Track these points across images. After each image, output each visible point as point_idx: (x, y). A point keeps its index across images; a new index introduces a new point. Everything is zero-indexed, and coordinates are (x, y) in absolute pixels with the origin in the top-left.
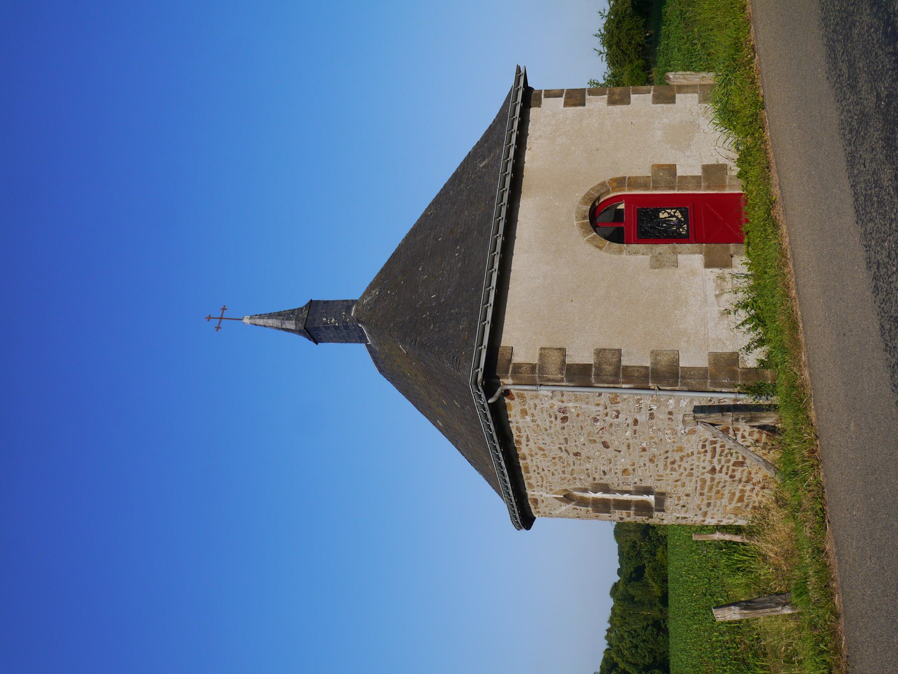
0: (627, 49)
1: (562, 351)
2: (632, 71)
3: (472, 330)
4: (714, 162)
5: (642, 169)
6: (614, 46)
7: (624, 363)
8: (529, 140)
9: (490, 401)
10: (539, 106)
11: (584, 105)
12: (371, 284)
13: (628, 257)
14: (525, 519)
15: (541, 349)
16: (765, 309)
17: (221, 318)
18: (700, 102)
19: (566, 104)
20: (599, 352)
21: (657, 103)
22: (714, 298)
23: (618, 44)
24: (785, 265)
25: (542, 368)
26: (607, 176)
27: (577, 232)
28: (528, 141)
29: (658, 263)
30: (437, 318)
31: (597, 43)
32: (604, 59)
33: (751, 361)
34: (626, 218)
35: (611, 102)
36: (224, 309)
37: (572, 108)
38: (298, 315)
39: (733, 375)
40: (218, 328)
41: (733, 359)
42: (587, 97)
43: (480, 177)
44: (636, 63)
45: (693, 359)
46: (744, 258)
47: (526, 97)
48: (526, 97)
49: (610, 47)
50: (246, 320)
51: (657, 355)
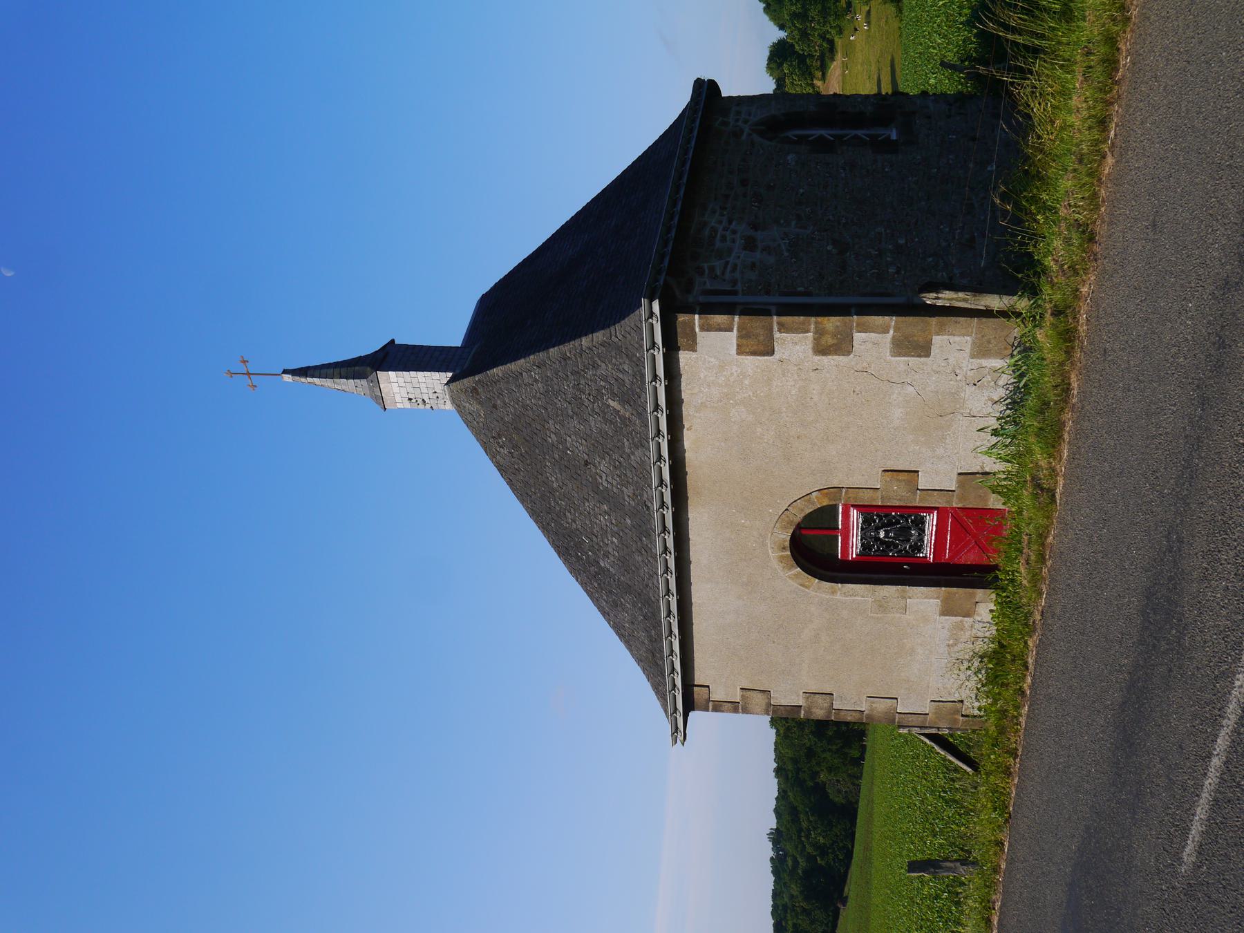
8: (687, 411)
18: (973, 356)
21: (900, 355)
42: (777, 335)
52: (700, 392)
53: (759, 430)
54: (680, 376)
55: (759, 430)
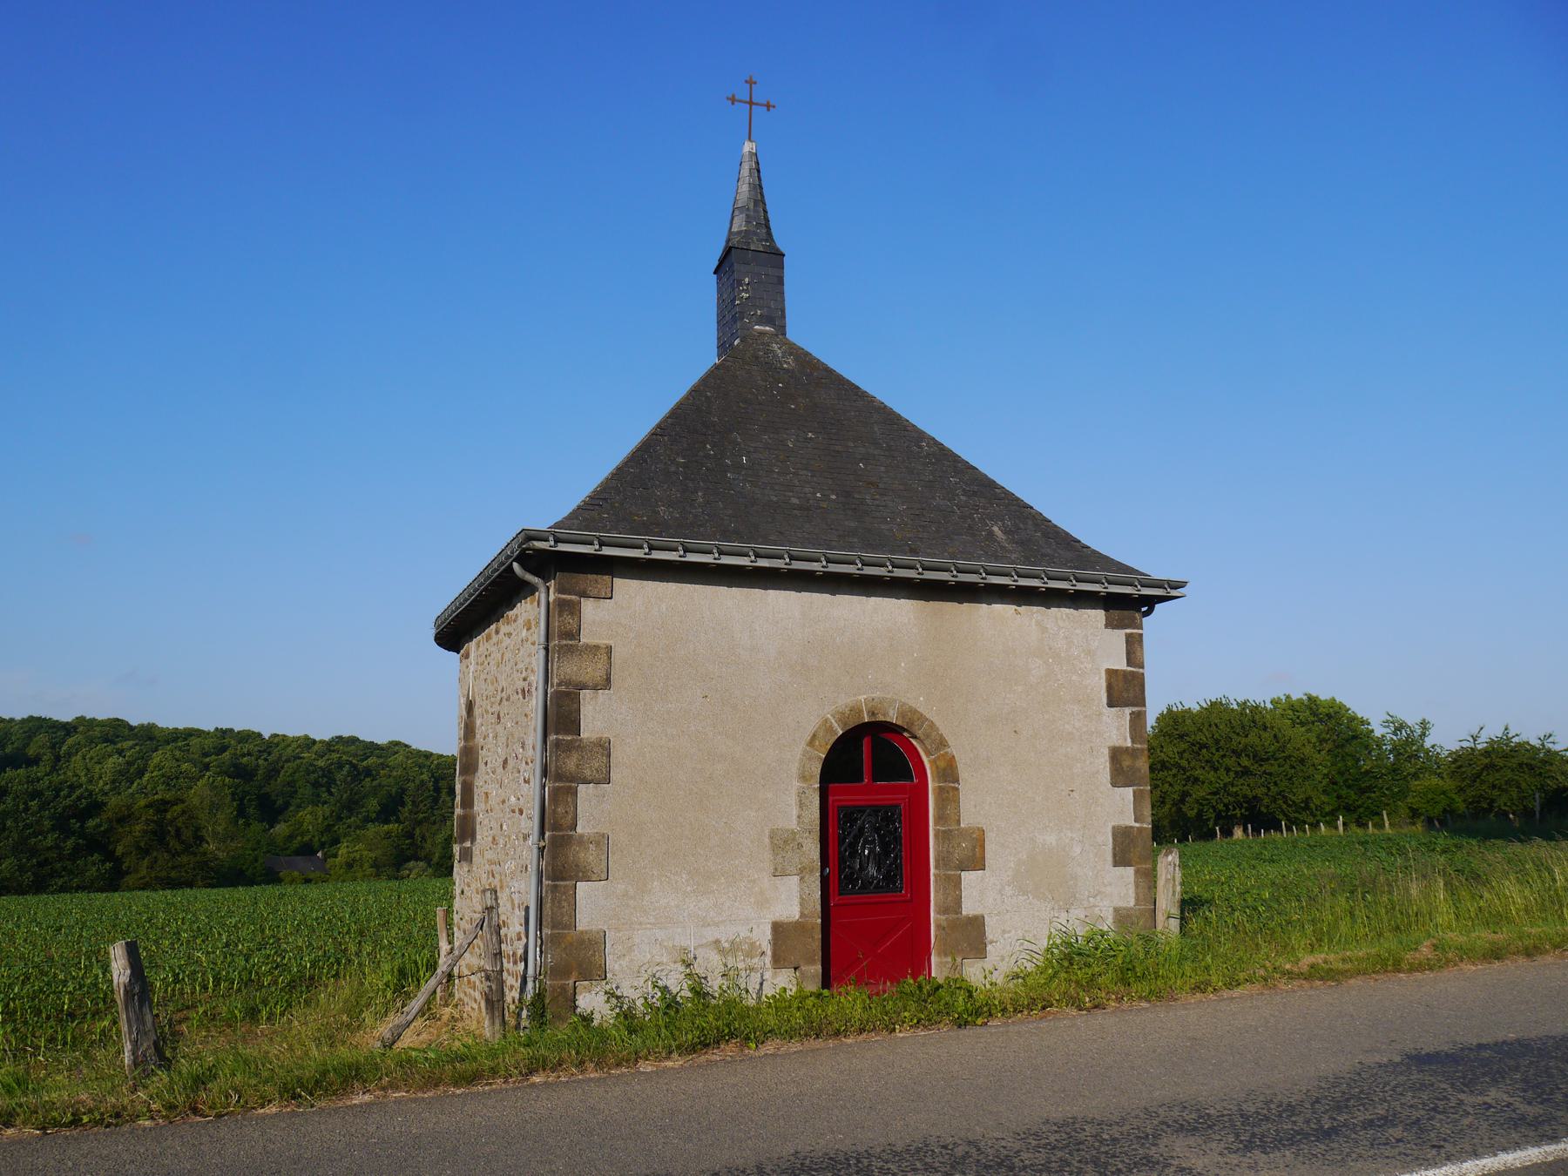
0: (1483, 782)
1: (607, 683)
2: (1444, 793)
3: (662, 528)
4: (989, 935)
5: (974, 807)
6: (1487, 761)
7: (581, 788)
9: (515, 565)
10: (1107, 626)
11: (1110, 705)
12: (807, 354)
13: (794, 791)
14: (455, 633)
15: (609, 649)
16: (700, 1023)
17: (751, 103)
18: (1116, 910)
19: (1111, 673)
20: (604, 747)
22: (711, 939)
23: (1490, 767)
24: (599, 1065)
25: (570, 650)
26: (959, 749)
27: (844, 701)
28: (1035, 608)
29: (781, 842)
30: (774, 469)
31: (1492, 732)
32: (1465, 744)
33: (591, 1000)
34: (875, 790)
35: (1116, 754)
36: (768, 106)
37: (1104, 684)
38: (755, 234)
39: (560, 971)
40: (733, 100)
41: (594, 971)
42: (1128, 711)
43: (970, 527)
44: (1458, 799)
45: (592, 905)
46: (793, 990)
47: (1129, 601)
48: (1129, 601)
49: (1486, 753)
50: (748, 147)
51: (598, 844)
52: (1060, 628)
53: (1020, 689)
54: (1076, 609)
55: (1020, 689)
